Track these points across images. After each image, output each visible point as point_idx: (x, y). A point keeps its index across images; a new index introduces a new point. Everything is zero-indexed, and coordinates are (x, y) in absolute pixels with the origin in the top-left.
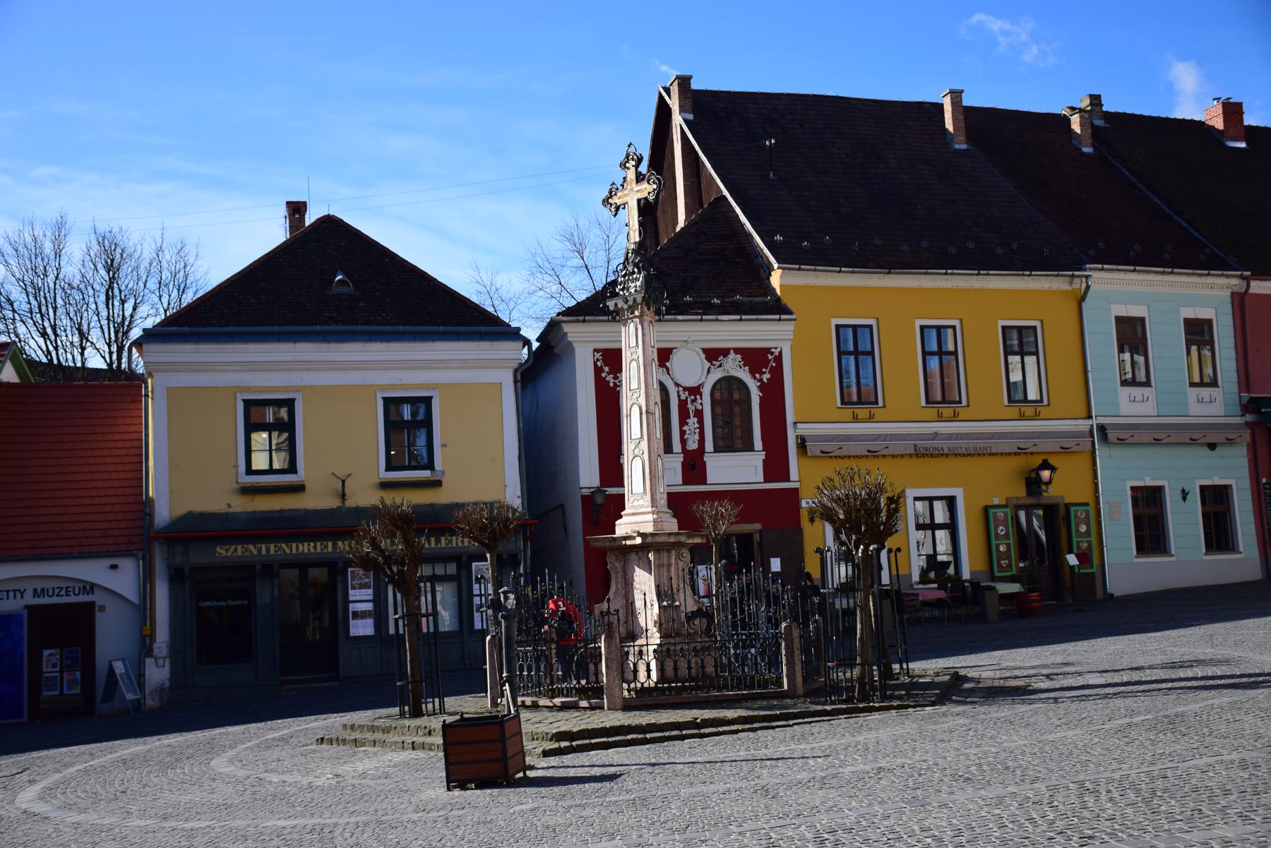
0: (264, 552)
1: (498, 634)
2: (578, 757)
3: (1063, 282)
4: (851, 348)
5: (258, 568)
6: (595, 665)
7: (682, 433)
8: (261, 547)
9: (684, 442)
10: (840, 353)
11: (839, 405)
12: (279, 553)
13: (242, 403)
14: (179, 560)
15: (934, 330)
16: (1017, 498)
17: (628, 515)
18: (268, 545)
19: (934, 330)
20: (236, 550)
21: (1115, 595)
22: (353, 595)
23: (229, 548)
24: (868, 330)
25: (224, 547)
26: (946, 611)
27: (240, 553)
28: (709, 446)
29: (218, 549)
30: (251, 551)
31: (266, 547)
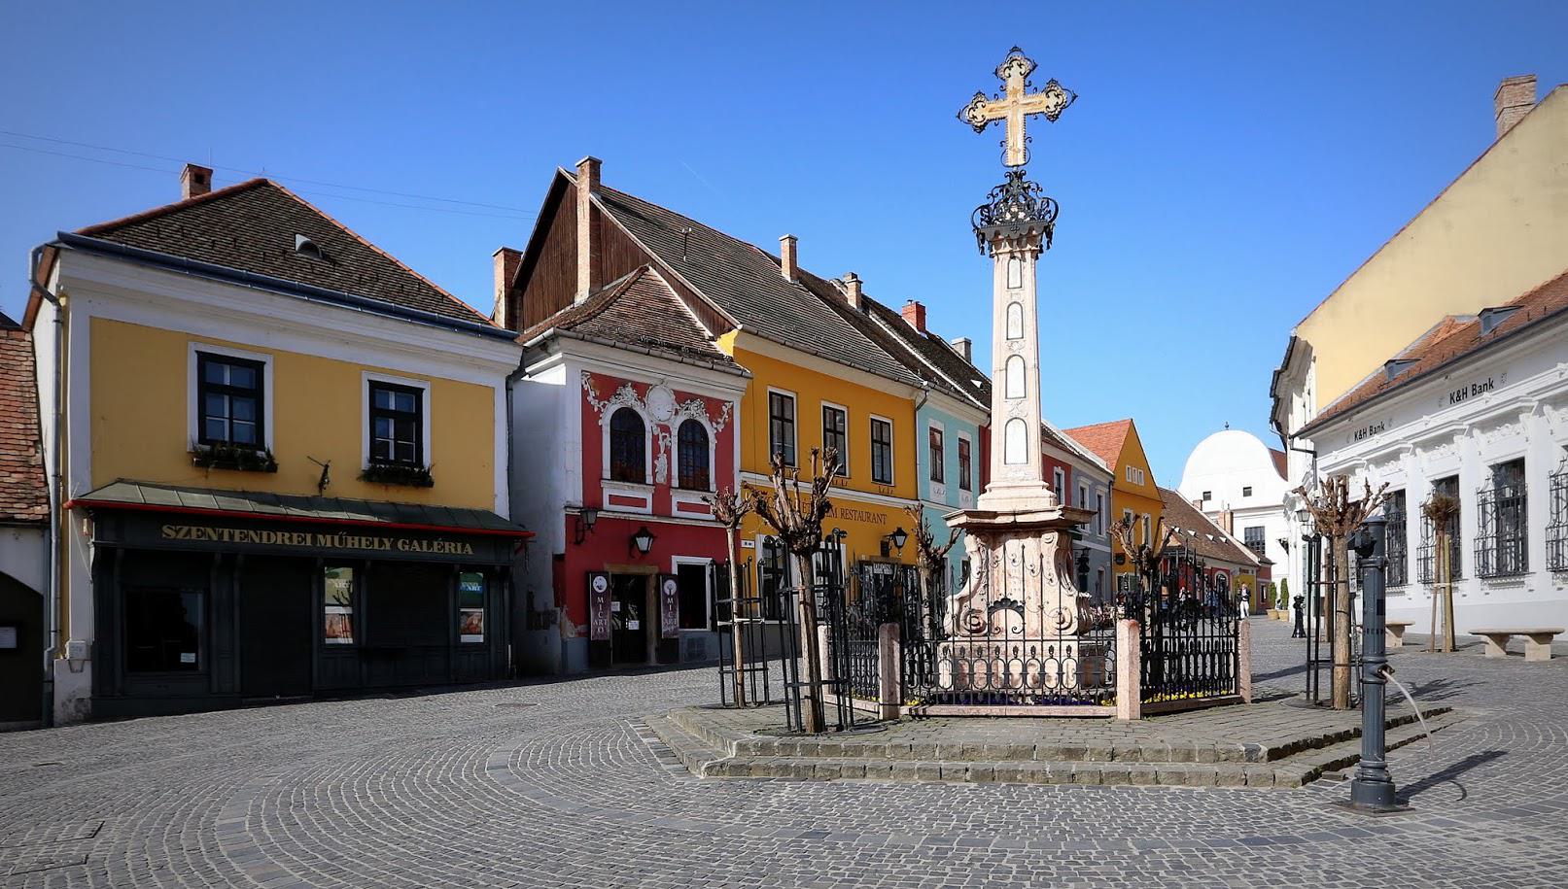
5: (218, 558)
7: (654, 466)
8: (223, 532)
9: (654, 474)
20: (189, 532)
28: (675, 483)
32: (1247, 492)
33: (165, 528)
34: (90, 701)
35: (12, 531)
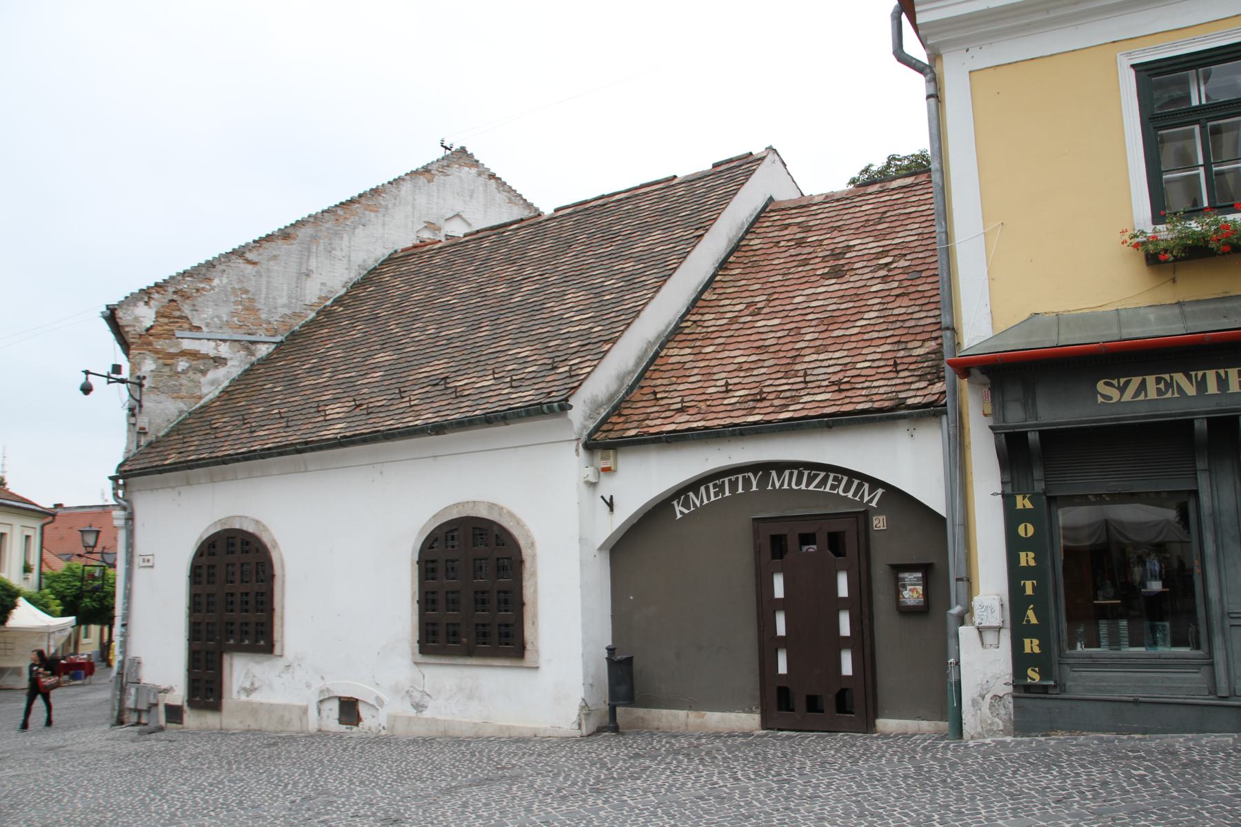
0: (1212, 388)
1: (1025, 802)
2: (419, 707)
3: (679, 727)
5: (1201, 426)
8: (1204, 376)
12: (1169, 395)
13: (1132, 73)
14: (1016, 416)
18: (1222, 372)
20: (1143, 386)
21: (7, 487)
23: (1127, 384)
25: (1115, 382)
27: (1152, 394)
29: (1101, 386)
30: (1180, 389)
31: (1218, 375)
32: (90, 526)
33: (1101, 386)
34: (1011, 699)
35: (904, 426)
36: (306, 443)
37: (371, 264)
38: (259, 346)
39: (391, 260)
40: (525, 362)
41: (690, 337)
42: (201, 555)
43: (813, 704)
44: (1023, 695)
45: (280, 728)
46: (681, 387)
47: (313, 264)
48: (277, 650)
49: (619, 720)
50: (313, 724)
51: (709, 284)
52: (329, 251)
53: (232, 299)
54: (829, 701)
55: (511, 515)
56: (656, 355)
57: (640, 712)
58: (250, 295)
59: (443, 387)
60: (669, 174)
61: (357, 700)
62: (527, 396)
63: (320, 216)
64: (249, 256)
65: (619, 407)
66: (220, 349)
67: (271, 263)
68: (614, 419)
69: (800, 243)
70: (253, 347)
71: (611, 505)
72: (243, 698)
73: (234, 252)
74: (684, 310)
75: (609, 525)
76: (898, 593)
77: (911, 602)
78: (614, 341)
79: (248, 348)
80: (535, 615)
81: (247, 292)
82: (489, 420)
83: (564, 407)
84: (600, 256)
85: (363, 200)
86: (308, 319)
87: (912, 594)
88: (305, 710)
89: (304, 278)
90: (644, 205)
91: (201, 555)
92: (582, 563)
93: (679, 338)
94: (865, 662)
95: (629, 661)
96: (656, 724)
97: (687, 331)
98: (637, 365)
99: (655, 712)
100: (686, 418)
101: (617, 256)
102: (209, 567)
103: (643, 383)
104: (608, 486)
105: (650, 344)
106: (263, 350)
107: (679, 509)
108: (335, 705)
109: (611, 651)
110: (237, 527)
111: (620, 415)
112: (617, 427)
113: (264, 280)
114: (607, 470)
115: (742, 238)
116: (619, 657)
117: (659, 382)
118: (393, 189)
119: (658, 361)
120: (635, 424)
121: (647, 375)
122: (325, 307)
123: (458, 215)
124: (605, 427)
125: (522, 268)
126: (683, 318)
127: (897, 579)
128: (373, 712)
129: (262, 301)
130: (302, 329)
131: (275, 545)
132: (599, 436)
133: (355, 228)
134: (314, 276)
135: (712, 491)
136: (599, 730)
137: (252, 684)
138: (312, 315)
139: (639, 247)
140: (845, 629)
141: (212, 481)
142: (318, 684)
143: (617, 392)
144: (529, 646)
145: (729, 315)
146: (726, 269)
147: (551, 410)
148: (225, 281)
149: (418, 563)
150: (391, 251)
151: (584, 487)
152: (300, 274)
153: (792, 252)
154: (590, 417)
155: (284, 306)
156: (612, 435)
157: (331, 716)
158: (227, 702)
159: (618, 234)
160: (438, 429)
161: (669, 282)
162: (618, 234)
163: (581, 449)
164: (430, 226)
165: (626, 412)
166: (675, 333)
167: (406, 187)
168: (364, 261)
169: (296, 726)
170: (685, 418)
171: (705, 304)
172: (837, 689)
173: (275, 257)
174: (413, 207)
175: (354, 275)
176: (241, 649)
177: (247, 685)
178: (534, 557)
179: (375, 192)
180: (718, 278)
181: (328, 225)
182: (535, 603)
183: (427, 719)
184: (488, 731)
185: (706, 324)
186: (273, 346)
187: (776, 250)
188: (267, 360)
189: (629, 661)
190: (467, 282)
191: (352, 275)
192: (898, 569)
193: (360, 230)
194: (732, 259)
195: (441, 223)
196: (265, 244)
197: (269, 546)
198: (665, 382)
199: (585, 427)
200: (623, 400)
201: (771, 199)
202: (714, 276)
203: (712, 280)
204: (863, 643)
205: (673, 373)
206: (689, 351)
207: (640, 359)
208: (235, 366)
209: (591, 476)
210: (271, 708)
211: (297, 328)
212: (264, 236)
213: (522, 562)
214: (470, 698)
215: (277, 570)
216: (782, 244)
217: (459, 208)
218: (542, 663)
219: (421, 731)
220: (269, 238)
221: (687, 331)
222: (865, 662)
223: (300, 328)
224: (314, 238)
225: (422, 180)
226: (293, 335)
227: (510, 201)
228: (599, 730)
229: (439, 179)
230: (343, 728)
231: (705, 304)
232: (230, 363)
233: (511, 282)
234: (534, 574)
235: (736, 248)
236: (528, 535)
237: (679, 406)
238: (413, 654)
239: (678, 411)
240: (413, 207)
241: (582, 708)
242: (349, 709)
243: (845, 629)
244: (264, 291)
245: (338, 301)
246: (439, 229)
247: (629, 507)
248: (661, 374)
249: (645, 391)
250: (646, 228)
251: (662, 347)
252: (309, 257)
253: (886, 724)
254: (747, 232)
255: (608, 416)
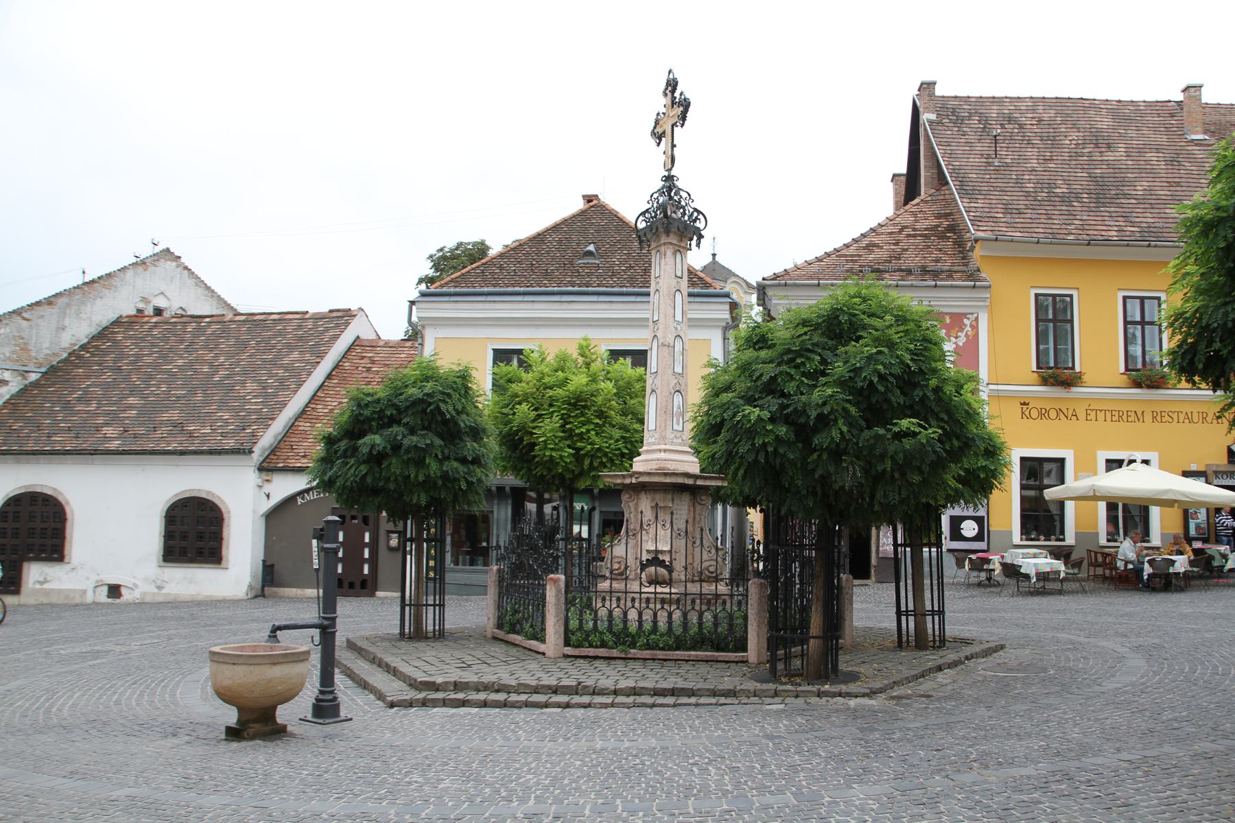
2: (159, 588)
4: (1138, 318)
5: (507, 489)
6: (582, 627)
10: (1126, 323)
11: (1035, 369)
15: (1138, 300)
16: (1217, 465)
17: (648, 452)
19: (1138, 300)
22: (951, 612)
24: (1156, 301)
26: (415, 501)
36: (96, 450)
37: (105, 323)
38: (31, 374)
39: (117, 322)
40: (227, 422)
41: (310, 417)
42: (8, 505)
43: (351, 585)
44: (751, 685)
45: (66, 602)
46: (304, 444)
47: (67, 322)
48: (66, 560)
49: (266, 593)
50: (89, 598)
51: (321, 386)
52: (78, 314)
53: (13, 342)
54: (358, 584)
55: (219, 498)
56: (293, 425)
57: (275, 589)
58: (25, 341)
59: (180, 429)
60: (304, 310)
61: (120, 585)
62: (230, 443)
63: (72, 290)
64: (25, 315)
65: (274, 451)
66: (5, 374)
67: (40, 320)
68: (272, 457)
69: (369, 370)
70: (26, 375)
71: (268, 496)
72: (38, 586)
73: (14, 312)
74: (308, 401)
75: (267, 505)
76: (388, 542)
77: (393, 546)
78: (273, 419)
79: (23, 375)
80: (228, 544)
81: (23, 338)
82: (211, 452)
83: (251, 452)
84: (264, 361)
85: (101, 281)
86: (62, 358)
87: (394, 542)
88: (85, 592)
89: (61, 331)
90: (289, 329)
91: (8, 505)
92: (253, 522)
93: (305, 416)
94: (374, 569)
95: (272, 566)
96: (282, 594)
97: (308, 413)
98: (283, 430)
99: (282, 589)
100: (306, 461)
101: (273, 363)
102: (15, 512)
103: (285, 439)
104: (268, 488)
105: (291, 419)
106: (33, 377)
107: (300, 501)
108: (105, 589)
109: (264, 561)
110: (39, 491)
111: (275, 455)
112: (274, 461)
113: (34, 331)
114: (268, 481)
115: (340, 361)
116: (268, 563)
117: (294, 439)
118: (121, 274)
119: (293, 428)
120: (282, 461)
121: (288, 434)
122: (74, 350)
123: (162, 293)
124: (267, 461)
125: (217, 356)
126: (306, 406)
127: (388, 536)
128: (130, 591)
129: (33, 345)
130: (60, 365)
131: (68, 503)
132: (265, 465)
133: (95, 299)
134: (67, 330)
135: (315, 494)
136: (256, 597)
137: (45, 579)
138: (65, 355)
139: (286, 361)
140: (366, 555)
141: (18, 463)
142: (94, 578)
143: (274, 443)
144: (224, 559)
145: (330, 407)
146: (330, 379)
147: (244, 453)
148: (8, 330)
149: (165, 517)
150: (118, 315)
151: (257, 488)
152: (58, 328)
153: (364, 375)
154: (261, 456)
155: (46, 348)
156: (271, 465)
157: (102, 596)
158: (24, 589)
159: (274, 347)
160: (182, 453)
161: (302, 388)
162: (274, 347)
163: (256, 471)
164: (144, 300)
165: (278, 454)
166: (302, 414)
167: (130, 273)
168: (101, 321)
169: (78, 600)
170: (306, 461)
171: (318, 398)
172: (361, 579)
173: (42, 317)
174: (134, 287)
175: (94, 330)
176: (38, 559)
177: (41, 579)
178: (229, 518)
179: (109, 275)
180: (326, 384)
181: (77, 297)
182: (228, 539)
183: (164, 594)
184: (200, 598)
185: (318, 411)
186: (40, 375)
187: (356, 372)
188: (35, 384)
189: (272, 566)
190: (182, 358)
191: (92, 330)
192: (390, 532)
193: (98, 301)
194: (334, 373)
195: (150, 298)
196: (36, 308)
197: (63, 503)
198: (297, 440)
199: (259, 460)
200: (276, 447)
201: (358, 337)
202: (324, 382)
203: (322, 385)
204: (373, 561)
205: (300, 436)
206: (308, 424)
207: (285, 427)
208: (15, 386)
209: (259, 482)
210: (60, 591)
211: (55, 363)
212: (33, 302)
213: (223, 519)
214: (190, 582)
215: (69, 516)
216: (360, 368)
217: (163, 289)
218: (230, 566)
219: (161, 599)
220: (38, 304)
221: (308, 413)
222: (374, 569)
223: (58, 363)
224: (68, 305)
225: (140, 269)
226: (53, 370)
227: (197, 285)
228: (256, 597)
229: (151, 269)
230: (110, 600)
231: (318, 398)
232: (10, 384)
233: (211, 365)
234: (229, 526)
235: (337, 366)
236: (227, 507)
237: (303, 454)
238: (159, 562)
239: (303, 456)
240: (134, 287)
241: (249, 586)
242: (114, 591)
243: (366, 555)
244: (34, 338)
245: (83, 347)
246: (149, 302)
247: (277, 498)
248: (294, 436)
249: (287, 443)
250: (290, 348)
251: (296, 420)
252: (64, 317)
253: (379, 594)
254: (343, 357)
255: (269, 455)
